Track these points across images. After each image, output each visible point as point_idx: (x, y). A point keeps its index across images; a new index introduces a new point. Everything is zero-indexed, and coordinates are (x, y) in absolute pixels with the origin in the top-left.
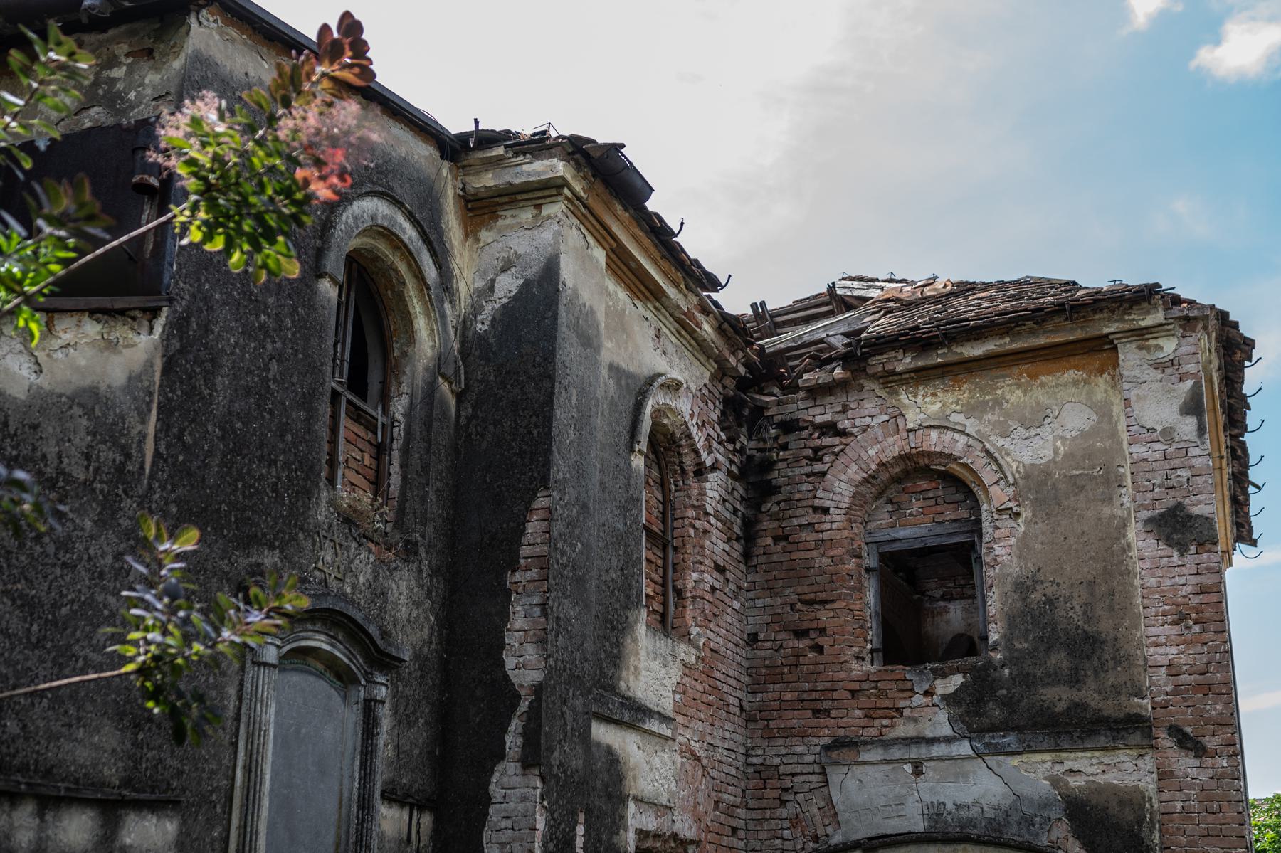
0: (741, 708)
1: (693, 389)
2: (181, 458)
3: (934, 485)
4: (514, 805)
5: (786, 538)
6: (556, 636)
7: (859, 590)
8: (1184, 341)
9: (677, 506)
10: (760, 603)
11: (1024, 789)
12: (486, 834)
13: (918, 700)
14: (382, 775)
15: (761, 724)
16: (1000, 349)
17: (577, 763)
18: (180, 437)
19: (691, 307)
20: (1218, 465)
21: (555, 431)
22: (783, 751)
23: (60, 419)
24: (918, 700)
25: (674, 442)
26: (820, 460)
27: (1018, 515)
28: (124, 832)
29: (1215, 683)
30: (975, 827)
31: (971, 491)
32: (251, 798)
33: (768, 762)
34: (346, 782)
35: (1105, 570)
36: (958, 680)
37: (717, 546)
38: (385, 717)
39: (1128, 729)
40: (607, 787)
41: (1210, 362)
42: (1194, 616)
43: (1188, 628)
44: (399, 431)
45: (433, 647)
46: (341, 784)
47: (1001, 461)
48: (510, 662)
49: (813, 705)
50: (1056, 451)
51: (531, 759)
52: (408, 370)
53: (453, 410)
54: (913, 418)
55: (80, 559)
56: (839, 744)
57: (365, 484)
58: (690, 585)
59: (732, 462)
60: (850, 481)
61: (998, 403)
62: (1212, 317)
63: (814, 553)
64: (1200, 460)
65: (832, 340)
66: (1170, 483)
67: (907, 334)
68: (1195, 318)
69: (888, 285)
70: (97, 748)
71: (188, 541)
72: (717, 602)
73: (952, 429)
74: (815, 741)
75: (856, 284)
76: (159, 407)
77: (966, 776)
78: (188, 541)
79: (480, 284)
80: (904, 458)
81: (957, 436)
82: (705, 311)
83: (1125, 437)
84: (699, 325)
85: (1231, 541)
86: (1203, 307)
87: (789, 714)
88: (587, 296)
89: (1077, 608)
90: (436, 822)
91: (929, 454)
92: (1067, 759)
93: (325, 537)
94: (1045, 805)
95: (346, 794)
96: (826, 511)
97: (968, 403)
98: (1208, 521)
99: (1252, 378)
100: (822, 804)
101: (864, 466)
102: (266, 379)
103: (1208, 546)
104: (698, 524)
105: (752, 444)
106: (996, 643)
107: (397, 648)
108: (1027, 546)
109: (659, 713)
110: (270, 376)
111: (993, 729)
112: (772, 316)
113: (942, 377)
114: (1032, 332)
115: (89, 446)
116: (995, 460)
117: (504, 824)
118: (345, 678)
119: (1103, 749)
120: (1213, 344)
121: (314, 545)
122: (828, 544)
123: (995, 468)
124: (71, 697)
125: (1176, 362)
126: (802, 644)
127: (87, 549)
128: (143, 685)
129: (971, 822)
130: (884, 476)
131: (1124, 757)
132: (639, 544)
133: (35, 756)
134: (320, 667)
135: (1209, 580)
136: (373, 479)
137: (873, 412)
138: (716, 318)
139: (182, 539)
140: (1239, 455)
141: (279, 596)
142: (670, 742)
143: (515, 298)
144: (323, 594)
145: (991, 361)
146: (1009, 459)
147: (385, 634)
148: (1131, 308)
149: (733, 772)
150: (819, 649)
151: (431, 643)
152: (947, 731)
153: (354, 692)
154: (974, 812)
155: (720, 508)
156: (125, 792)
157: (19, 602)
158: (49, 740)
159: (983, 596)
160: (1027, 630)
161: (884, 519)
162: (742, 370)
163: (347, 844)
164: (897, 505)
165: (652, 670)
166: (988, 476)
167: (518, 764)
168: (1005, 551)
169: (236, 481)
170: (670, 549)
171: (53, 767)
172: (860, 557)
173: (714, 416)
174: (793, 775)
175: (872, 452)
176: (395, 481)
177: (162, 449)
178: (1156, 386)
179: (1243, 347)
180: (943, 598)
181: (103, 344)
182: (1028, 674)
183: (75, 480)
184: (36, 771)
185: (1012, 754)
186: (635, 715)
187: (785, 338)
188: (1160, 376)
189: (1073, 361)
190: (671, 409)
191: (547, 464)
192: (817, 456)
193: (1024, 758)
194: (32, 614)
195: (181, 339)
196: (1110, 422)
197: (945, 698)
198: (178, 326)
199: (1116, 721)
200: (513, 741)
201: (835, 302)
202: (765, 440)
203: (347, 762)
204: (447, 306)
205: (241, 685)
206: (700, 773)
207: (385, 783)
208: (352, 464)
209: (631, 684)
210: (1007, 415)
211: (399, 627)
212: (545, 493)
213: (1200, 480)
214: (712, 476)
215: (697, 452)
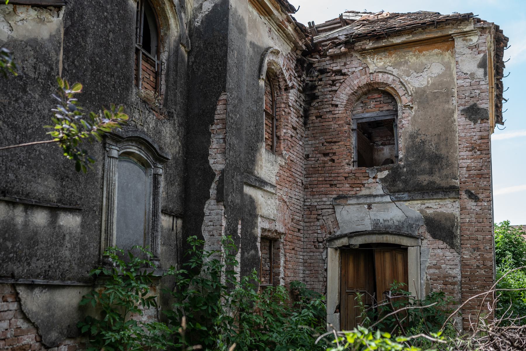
0: (302, 183)
1: (284, 54)
2: (74, 71)
3: (379, 96)
4: (214, 217)
5: (321, 117)
6: (230, 151)
7: (349, 138)
8: (481, 37)
9: (277, 103)
10: (310, 142)
11: (410, 214)
12: (203, 228)
13: (371, 180)
14: (161, 204)
15: (310, 190)
16: (407, 40)
17: (238, 201)
18: (73, 63)
19: (284, 19)
20: (491, 91)
21: (228, 68)
22: (318, 200)
23: (22, 51)
24: (371, 180)
25: (276, 76)
26: (335, 85)
27: (412, 108)
28: (60, 220)
29: (484, 174)
30: (390, 228)
31: (394, 98)
32: (110, 209)
33: (312, 204)
34: (147, 206)
35: (445, 130)
36: (386, 173)
37: (293, 119)
38: (162, 179)
39: (451, 191)
40: (250, 211)
41: (491, 47)
42: (478, 148)
43: (475, 152)
44: (164, 67)
45: (180, 155)
46: (145, 206)
47: (406, 86)
48: (211, 161)
49: (330, 182)
50: (428, 82)
51: (220, 199)
52: (167, 41)
53: (186, 59)
54: (372, 68)
55: (35, 110)
56: (340, 197)
57: (151, 88)
58: (282, 134)
59: (300, 85)
60: (346, 94)
61: (406, 62)
62: (492, 28)
63: (332, 123)
64: (484, 86)
65: (340, 37)
66: (472, 95)
67: (371, 33)
68: (486, 28)
69: (364, 15)
70: (47, 186)
71: (78, 89)
72: (293, 142)
73: (388, 73)
74: (331, 196)
75: (351, 14)
76: (64, 49)
77: (388, 209)
78: (78, 89)
79: (196, 5)
80: (368, 84)
81: (389, 76)
82: (289, 21)
83: (455, 76)
84: (287, 27)
85: (494, 123)
86: (489, 23)
87: (321, 186)
88: (241, 12)
89: (433, 145)
90: (184, 223)
91: (378, 83)
92: (427, 203)
93: (135, 108)
94: (418, 220)
95: (147, 210)
96: (337, 106)
97: (394, 62)
98: (486, 110)
99: (507, 54)
100: (333, 220)
101: (352, 88)
102: (108, 40)
103: (485, 121)
104: (286, 110)
105: (308, 79)
106: (401, 158)
107: (166, 154)
108: (415, 120)
109: (270, 184)
110: (110, 39)
111: (399, 191)
112: (316, 28)
113: (384, 51)
114: (421, 33)
115: (35, 64)
116: (404, 86)
117: (210, 223)
118: (145, 165)
119: (440, 199)
120: (492, 39)
121: (131, 111)
122: (337, 119)
123: (404, 89)
124: (35, 166)
125: (477, 46)
126: (326, 159)
127: (37, 106)
128: (62, 147)
129: (389, 227)
130: (360, 92)
131: (448, 202)
132: (262, 116)
133: (22, 188)
134: (136, 160)
135: (485, 134)
136: (154, 87)
137: (356, 66)
138: (293, 24)
139: (75, 88)
140: (499, 87)
141: (116, 115)
142: (274, 195)
143: (211, 12)
144: (135, 131)
145: (404, 45)
146: (409, 85)
147: (161, 148)
148: (461, 23)
149: (299, 208)
150: (333, 161)
151: (179, 153)
152: (381, 192)
153: (149, 171)
154: (390, 223)
155: (294, 104)
156: (59, 204)
157: (10, 126)
158: (27, 182)
159: (397, 140)
160: (414, 153)
161: (359, 109)
162: (304, 47)
163: (149, 229)
164: (365, 104)
165: (267, 167)
166: (401, 92)
167: (215, 201)
168: (407, 122)
169: (98, 82)
170: (275, 120)
171: (29, 193)
172: (350, 125)
173: (293, 66)
174: (322, 209)
175: (355, 82)
176: (163, 88)
177: (66, 67)
178: (469, 56)
179: (504, 41)
180: (382, 144)
181: (38, 20)
182: (413, 170)
183: (30, 78)
184: (22, 194)
185: (406, 201)
186: (261, 184)
187: (322, 37)
188: (471, 52)
189: (437, 45)
190: (275, 62)
191: (225, 81)
192: (333, 83)
193: (410, 202)
194: (16, 132)
195: (71, 21)
196: (450, 70)
197: (381, 179)
198: (69, 15)
199: (446, 189)
200: (213, 192)
201: (342, 22)
202: (313, 77)
203: (147, 198)
204: (183, 14)
205: (104, 165)
206: (286, 207)
207: (163, 207)
208: (145, 80)
209: (259, 172)
210: (410, 67)
211: (167, 146)
212: (224, 93)
213: (483, 94)
214: (292, 91)
215: (285, 81)
